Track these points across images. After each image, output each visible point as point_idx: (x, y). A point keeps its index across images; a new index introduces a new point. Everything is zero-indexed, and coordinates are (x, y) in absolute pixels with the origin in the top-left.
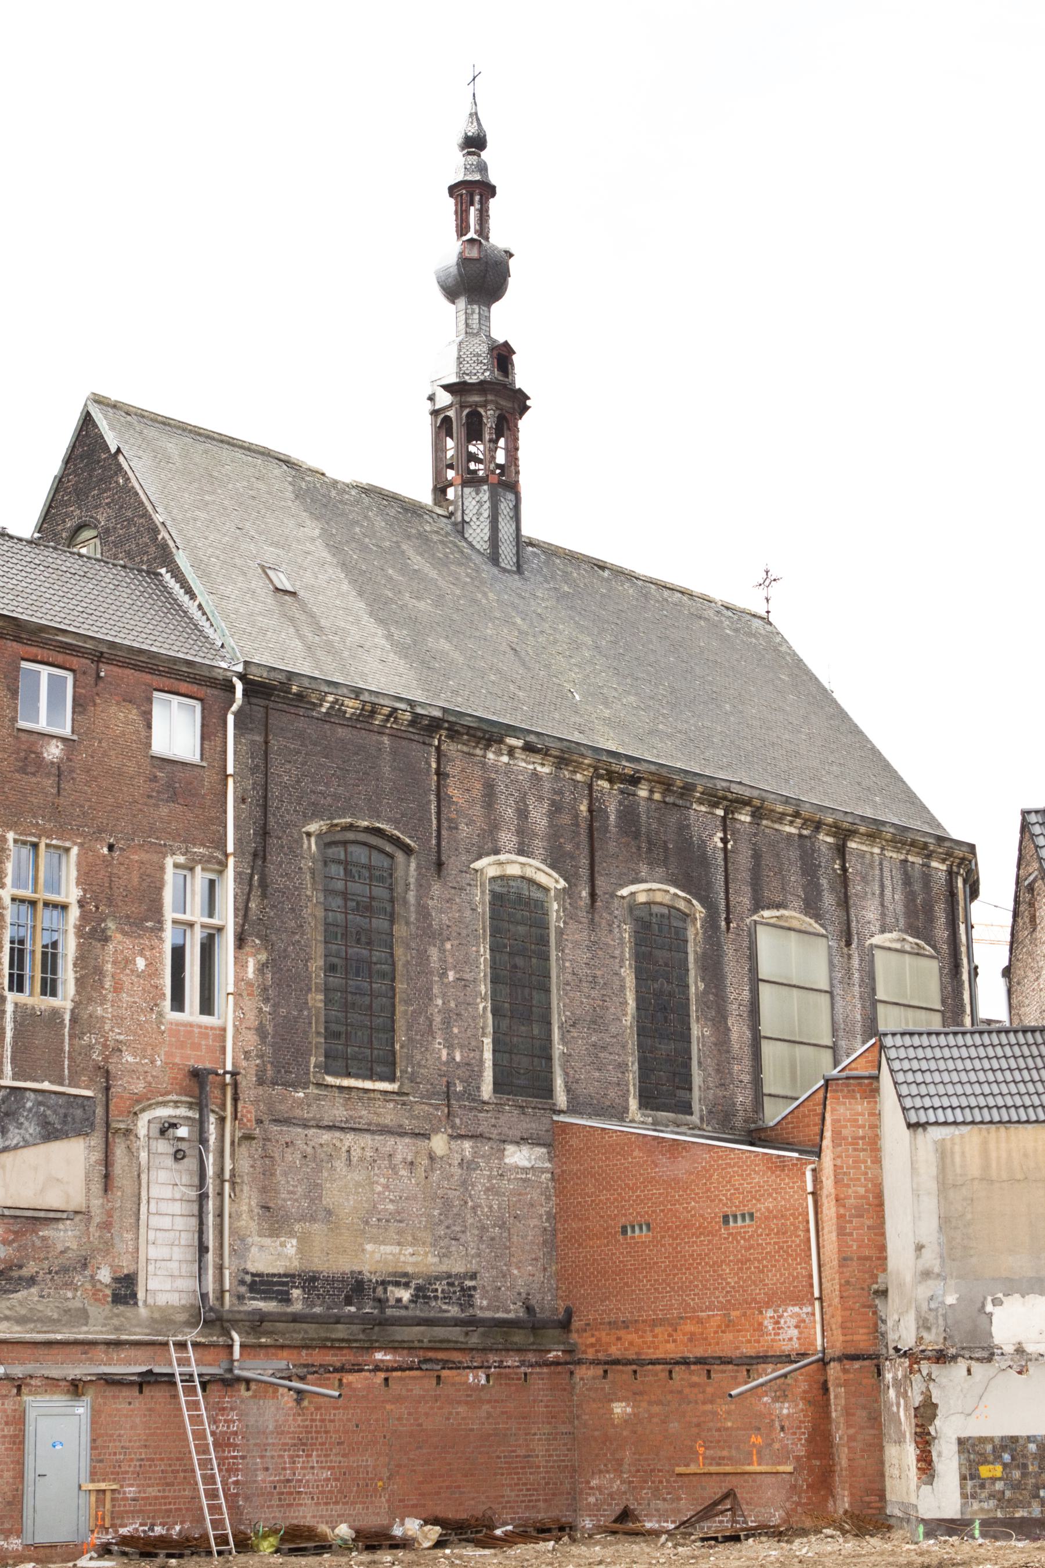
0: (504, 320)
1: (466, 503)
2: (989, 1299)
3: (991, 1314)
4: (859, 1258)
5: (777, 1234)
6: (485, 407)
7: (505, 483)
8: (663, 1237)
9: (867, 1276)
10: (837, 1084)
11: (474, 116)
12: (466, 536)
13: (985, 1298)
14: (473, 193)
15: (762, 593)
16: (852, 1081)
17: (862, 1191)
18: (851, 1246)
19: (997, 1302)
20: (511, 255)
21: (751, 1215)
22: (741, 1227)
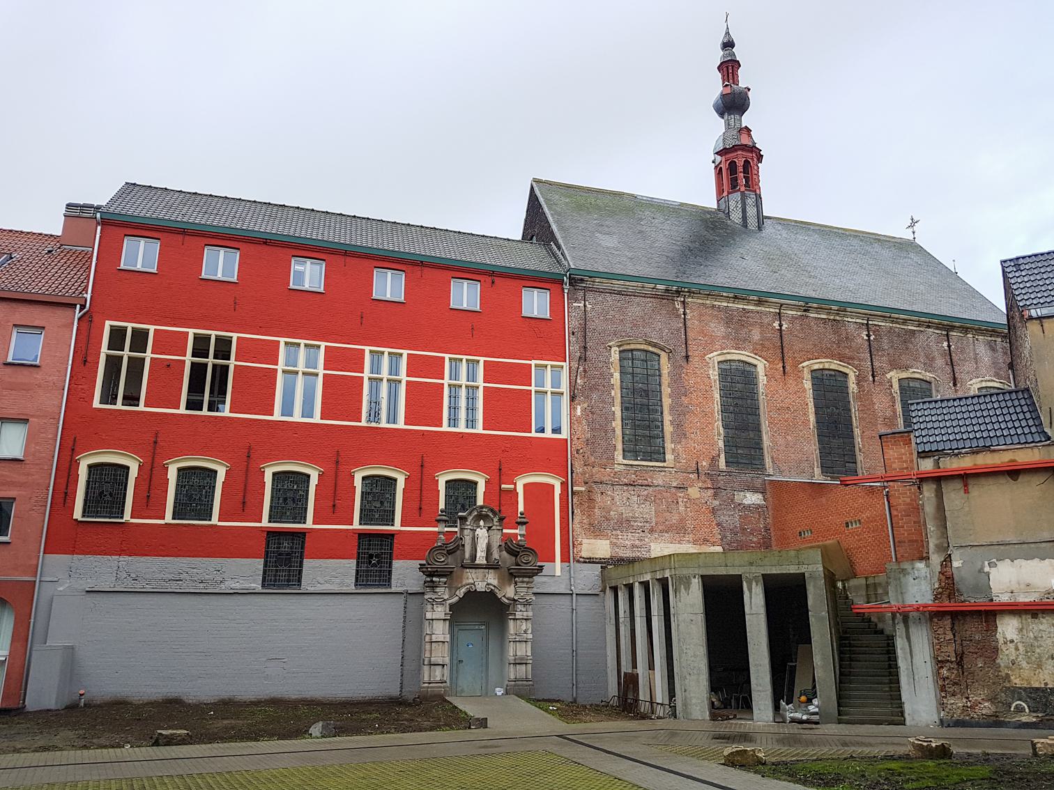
2: (986, 563)
3: (988, 574)
4: (909, 541)
8: (818, 537)
10: (887, 438)
11: (727, 33)
12: (731, 218)
13: (983, 563)
14: (729, 68)
15: (911, 230)
16: (896, 435)
17: (908, 500)
18: (904, 534)
20: (749, 90)
21: (859, 520)
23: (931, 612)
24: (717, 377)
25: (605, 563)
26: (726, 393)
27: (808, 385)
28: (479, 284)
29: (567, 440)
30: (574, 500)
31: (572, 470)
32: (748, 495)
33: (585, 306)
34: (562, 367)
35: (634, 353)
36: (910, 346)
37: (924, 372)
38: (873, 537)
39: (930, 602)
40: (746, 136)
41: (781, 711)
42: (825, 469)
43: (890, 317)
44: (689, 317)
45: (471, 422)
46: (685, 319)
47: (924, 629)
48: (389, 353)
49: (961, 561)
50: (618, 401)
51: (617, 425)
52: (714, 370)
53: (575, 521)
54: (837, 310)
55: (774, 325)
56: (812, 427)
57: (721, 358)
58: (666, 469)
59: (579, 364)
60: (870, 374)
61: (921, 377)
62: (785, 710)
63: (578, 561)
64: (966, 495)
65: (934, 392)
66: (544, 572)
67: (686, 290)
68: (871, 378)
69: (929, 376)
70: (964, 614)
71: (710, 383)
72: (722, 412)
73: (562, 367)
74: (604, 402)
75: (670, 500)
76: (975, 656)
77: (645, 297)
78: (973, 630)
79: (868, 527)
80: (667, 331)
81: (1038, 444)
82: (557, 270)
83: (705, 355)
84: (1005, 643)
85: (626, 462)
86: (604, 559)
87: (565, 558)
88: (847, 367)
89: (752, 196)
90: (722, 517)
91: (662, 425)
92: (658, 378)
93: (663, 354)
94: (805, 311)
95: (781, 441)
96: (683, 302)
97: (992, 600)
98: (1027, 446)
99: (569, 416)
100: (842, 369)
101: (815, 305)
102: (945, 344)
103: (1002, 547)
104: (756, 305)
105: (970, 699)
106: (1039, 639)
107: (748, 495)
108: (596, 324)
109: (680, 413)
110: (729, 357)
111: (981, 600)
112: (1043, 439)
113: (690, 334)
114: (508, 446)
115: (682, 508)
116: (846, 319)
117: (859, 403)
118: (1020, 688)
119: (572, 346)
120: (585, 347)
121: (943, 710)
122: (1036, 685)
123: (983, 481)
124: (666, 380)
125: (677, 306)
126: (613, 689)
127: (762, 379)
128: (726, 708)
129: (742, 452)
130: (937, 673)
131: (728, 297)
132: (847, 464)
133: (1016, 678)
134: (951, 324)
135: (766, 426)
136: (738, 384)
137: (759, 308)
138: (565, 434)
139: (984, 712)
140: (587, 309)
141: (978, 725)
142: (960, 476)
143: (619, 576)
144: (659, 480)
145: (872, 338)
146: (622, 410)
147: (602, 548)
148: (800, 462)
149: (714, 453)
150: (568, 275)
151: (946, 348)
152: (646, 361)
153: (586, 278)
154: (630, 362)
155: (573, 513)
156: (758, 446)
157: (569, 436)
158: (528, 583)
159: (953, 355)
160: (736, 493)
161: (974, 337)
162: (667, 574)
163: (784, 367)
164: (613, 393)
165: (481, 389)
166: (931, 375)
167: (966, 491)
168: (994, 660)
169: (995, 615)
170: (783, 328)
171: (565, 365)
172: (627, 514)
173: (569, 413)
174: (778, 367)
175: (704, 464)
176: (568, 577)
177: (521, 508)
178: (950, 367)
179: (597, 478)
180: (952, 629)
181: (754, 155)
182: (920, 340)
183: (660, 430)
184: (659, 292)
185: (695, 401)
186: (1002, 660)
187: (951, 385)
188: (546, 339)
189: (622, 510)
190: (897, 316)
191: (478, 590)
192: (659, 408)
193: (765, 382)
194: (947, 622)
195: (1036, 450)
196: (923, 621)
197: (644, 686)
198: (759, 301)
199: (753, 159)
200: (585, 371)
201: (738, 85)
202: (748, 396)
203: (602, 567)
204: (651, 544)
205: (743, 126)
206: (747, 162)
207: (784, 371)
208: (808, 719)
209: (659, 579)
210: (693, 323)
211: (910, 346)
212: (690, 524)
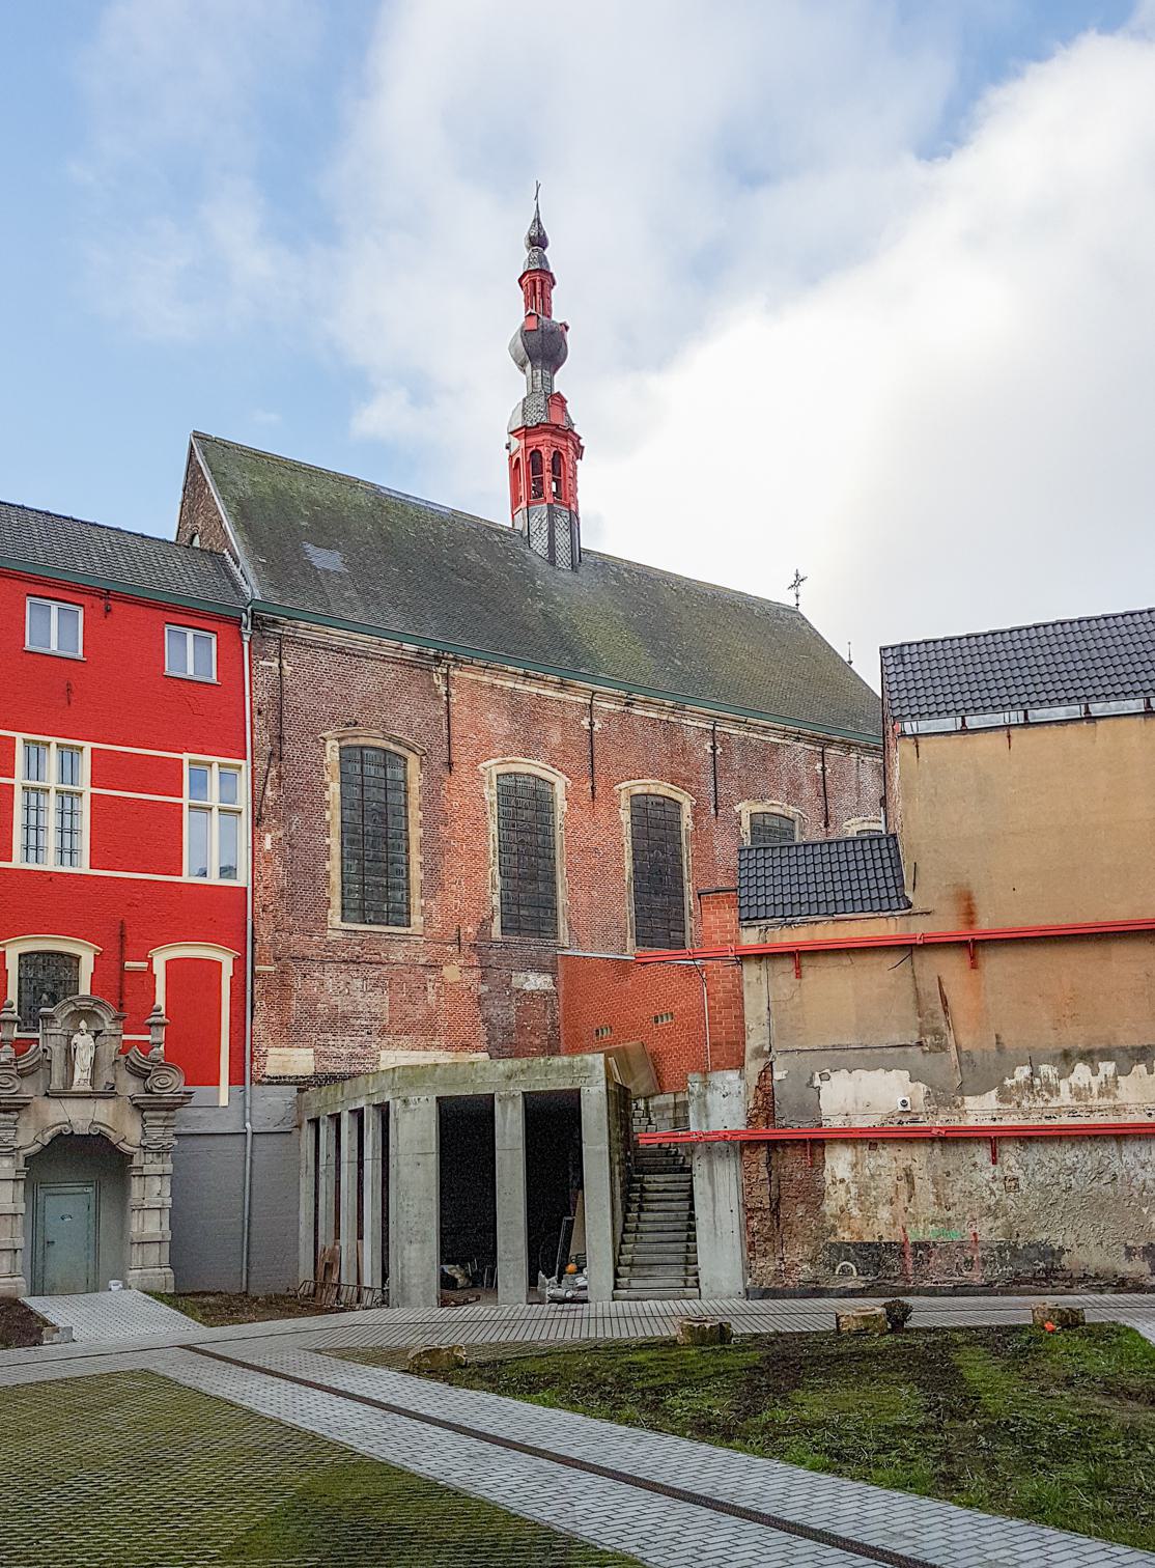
0: (561, 382)
1: (531, 522)
2: (817, 1074)
5: (688, 1028)
6: (546, 456)
7: (565, 497)
9: (735, 1058)
11: (537, 221)
13: (813, 1074)
14: (538, 283)
15: (793, 591)
16: (721, 894)
19: (825, 1077)
21: (672, 1014)
22: (666, 1025)
23: (742, 1142)
24: (495, 798)
25: (304, 1082)
26: (508, 822)
27: (625, 816)
28: (214, 640)
29: (246, 888)
30: (256, 986)
31: (253, 938)
32: (531, 977)
33: (281, 667)
34: (240, 767)
35: (365, 752)
36: (771, 766)
37: (785, 805)
38: (687, 1036)
39: (743, 1128)
40: (559, 410)
41: (538, 1288)
42: (642, 939)
43: (745, 722)
44: (455, 701)
45: (66, 852)
46: (448, 703)
47: (733, 1164)
48: (58, 745)
49: (785, 1072)
50: (336, 829)
51: (334, 866)
52: (491, 787)
53: (256, 1019)
54: (673, 707)
55: (583, 722)
56: (627, 879)
57: (503, 769)
58: (411, 938)
59: (269, 765)
60: (713, 804)
61: (782, 813)
62: (544, 1286)
63: (260, 1082)
64: (798, 981)
65: (797, 833)
66: (193, 1102)
67: (451, 656)
68: (713, 811)
69: (791, 811)
70: (783, 1143)
71: (484, 807)
72: (500, 851)
73: (240, 767)
74: (312, 829)
75: (413, 985)
76: (795, 1201)
77: (384, 661)
78: (793, 1164)
79: (682, 1022)
80: (418, 720)
81: (896, 913)
82: (230, 599)
83: (478, 762)
84: (834, 1183)
85: (345, 926)
86: (303, 1077)
87: (237, 1078)
88: (681, 793)
89: (564, 514)
90: (492, 1009)
91: (408, 869)
92: (402, 795)
93: (411, 757)
94: (627, 704)
95: (583, 899)
96: (446, 676)
97: (821, 1125)
98: (881, 914)
99: (250, 850)
100: (673, 795)
101: (642, 697)
102: (819, 766)
103: (838, 1053)
104: (558, 690)
105: (785, 1260)
106: (877, 1177)
107: (531, 977)
108: (300, 700)
109: (436, 850)
110: (514, 768)
111: (807, 1125)
112: (903, 907)
113: (457, 729)
114: (139, 896)
115: (432, 998)
116: (684, 721)
117: (694, 846)
118: (848, 1244)
119: (257, 733)
120: (280, 737)
121: (750, 1277)
122: (868, 1239)
123: (821, 961)
124: (415, 798)
125: (436, 681)
126: (306, 1271)
127: (561, 805)
128: (476, 1286)
129: (527, 913)
130: (745, 1227)
131: (515, 674)
132: (672, 934)
133: (844, 1231)
134: (829, 737)
135: (562, 875)
136: (526, 811)
137: (560, 695)
138: (242, 879)
139: (801, 1277)
140: (283, 673)
141: (793, 1295)
142: (791, 954)
143: (319, 1101)
144: (398, 955)
145: (718, 752)
146: (342, 843)
147: (300, 1060)
148: (608, 928)
149: (485, 914)
150: (249, 609)
151: (820, 772)
152: (385, 767)
153: (282, 620)
154: (358, 766)
155: (253, 1007)
156: (550, 905)
157: (250, 882)
158: (166, 1118)
159: (828, 781)
160: (514, 974)
161: (858, 758)
162: (388, 1097)
163: (592, 788)
164: (328, 815)
165: (87, 799)
166: (796, 810)
167: (799, 976)
168: (818, 1207)
169: (823, 1145)
170: (595, 729)
171: (246, 764)
172: (343, 1005)
173: (250, 845)
174: (585, 787)
175: (470, 930)
176: (240, 1108)
177: (160, 1000)
178: (823, 799)
179: (296, 951)
180: (767, 1165)
181: (570, 445)
182: (784, 758)
183: (404, 876)
184: (407, 655)
185: (459, 834)
186: (830, 1207)
187: (822, 825)
188: (210, 717)
189: (337, 1000)
190: (755, 721)
191: (76, 1133)
192: (404, 844)
193: (565, 810)
194: (762, 1154)
195: (891, 920)
196: (732, 1155)
197: (348, 1262)
198: (561, 684)
199: (566, 450)
200: (280, 776)
201: (549, 317)
202: (540, 829)
203: (299, 1090)
204: (382, 1053)
205: (556, 392)
206: (558, 454)
207: (593, 793)
208: (573, 1297)
209: (377, 1105)
210: (460, 711)
211: (771, 766)
212: (442, 1021)
